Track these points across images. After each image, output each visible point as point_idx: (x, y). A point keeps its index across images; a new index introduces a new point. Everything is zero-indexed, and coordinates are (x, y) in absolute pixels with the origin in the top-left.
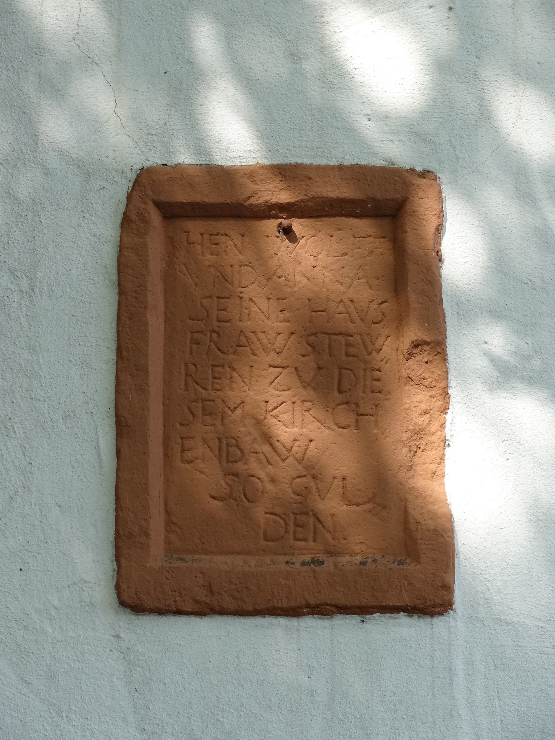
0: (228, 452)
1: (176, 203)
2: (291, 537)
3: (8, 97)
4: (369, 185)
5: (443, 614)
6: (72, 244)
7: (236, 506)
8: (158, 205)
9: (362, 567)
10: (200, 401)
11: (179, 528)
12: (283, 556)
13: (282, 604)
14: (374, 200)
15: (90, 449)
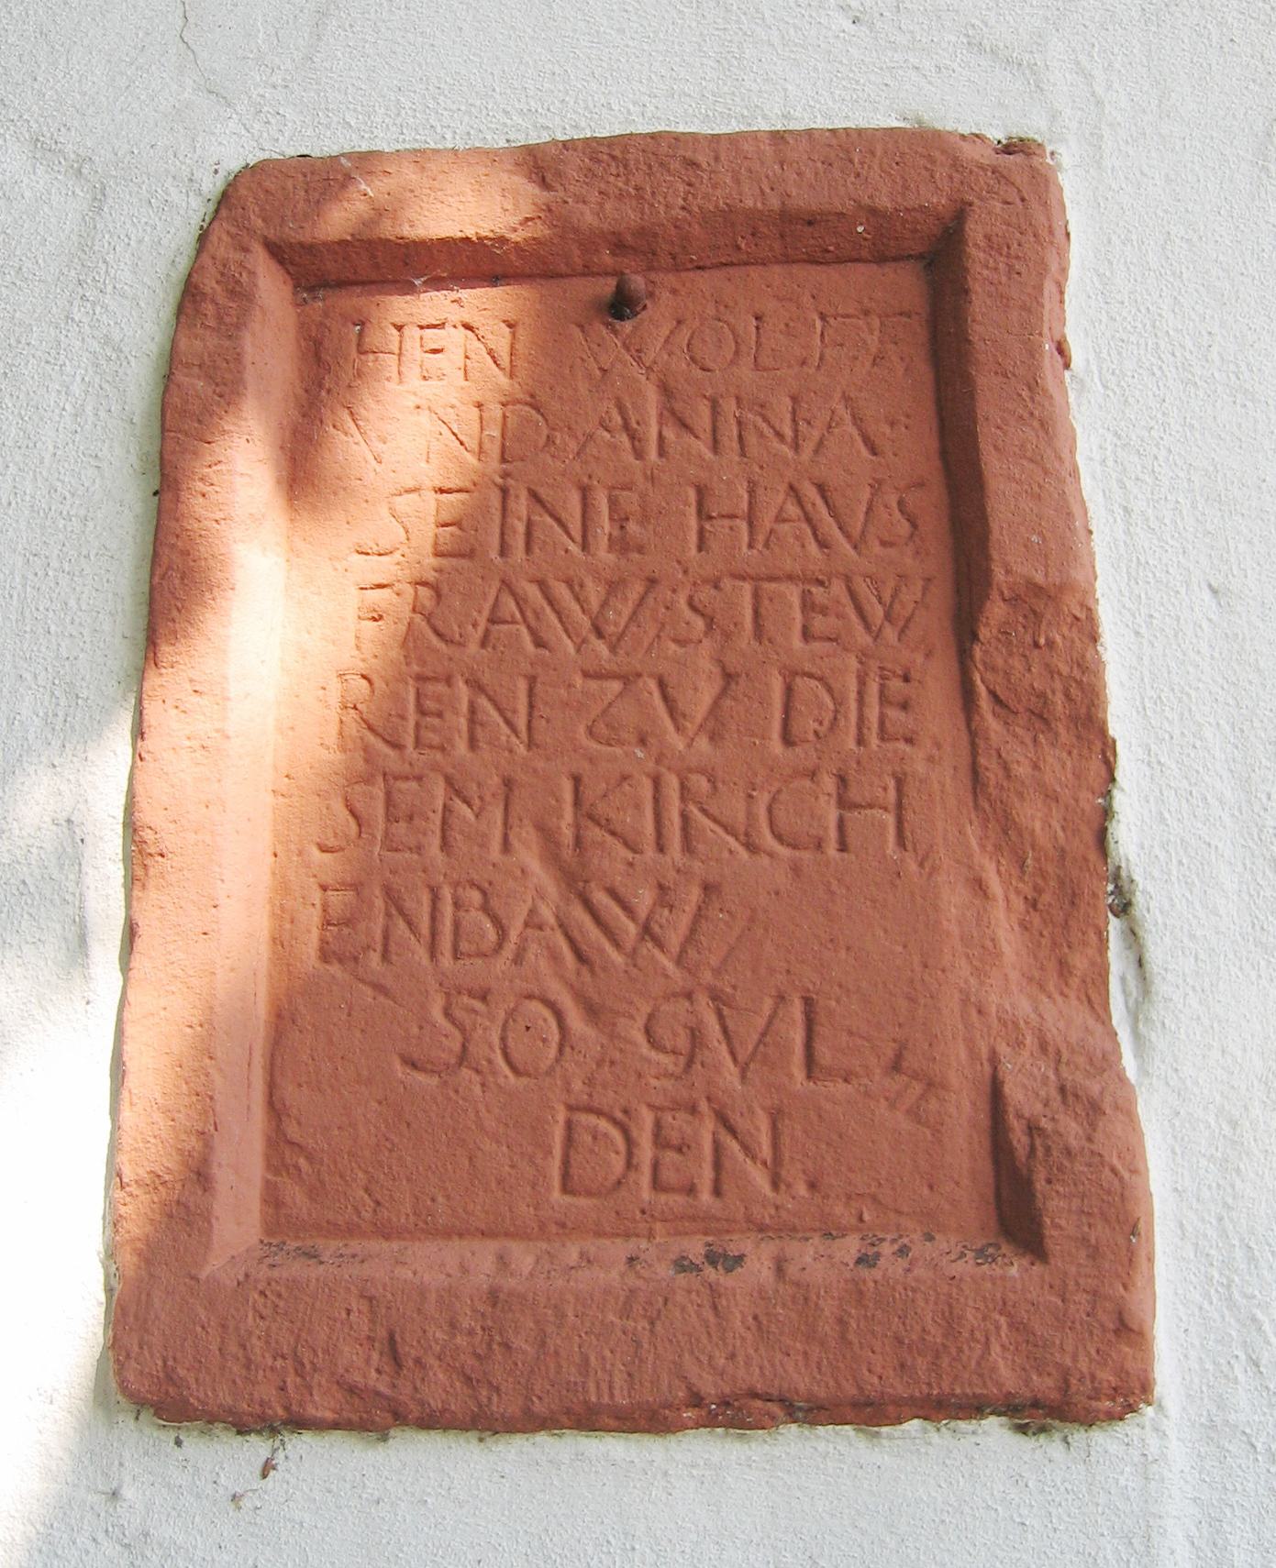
0: (457, 925)
1: (325, 244)
2: (646, 1179)
3: (533, 592)
4: (858, 175)
5: (1121, 1419)
6: (48, 367)
7: (477, 1090)
8: (277, 251)
9: (865, 1272)
10: (380, 779)
11: (310, 1158)
12: (618, 1241)
13: (599, 1396)
14: (873, 211)
15: (58, 927)
